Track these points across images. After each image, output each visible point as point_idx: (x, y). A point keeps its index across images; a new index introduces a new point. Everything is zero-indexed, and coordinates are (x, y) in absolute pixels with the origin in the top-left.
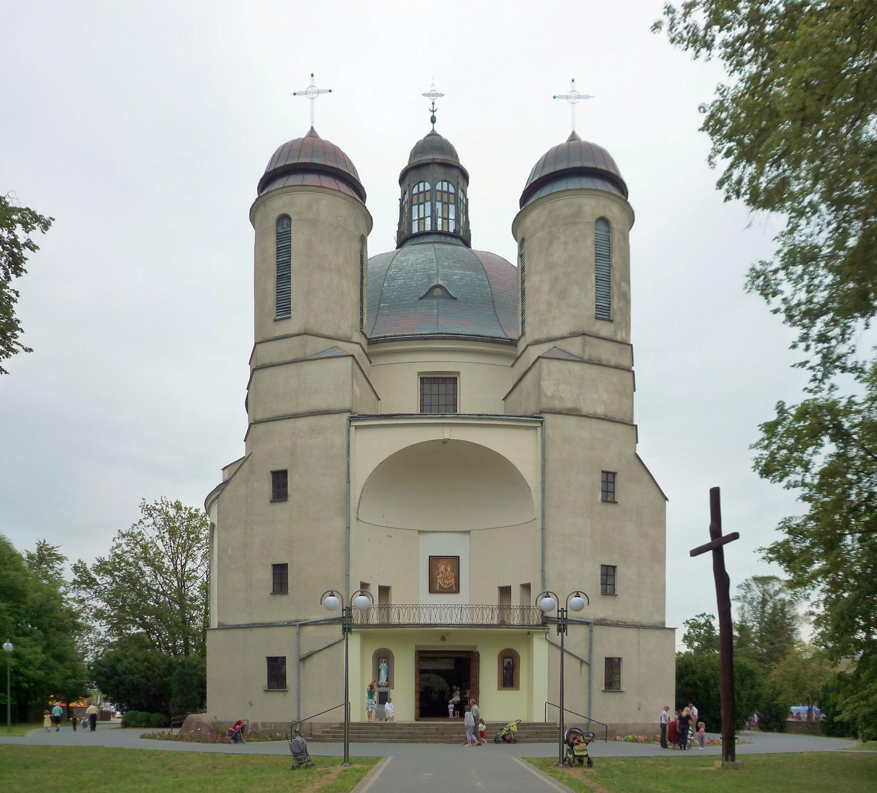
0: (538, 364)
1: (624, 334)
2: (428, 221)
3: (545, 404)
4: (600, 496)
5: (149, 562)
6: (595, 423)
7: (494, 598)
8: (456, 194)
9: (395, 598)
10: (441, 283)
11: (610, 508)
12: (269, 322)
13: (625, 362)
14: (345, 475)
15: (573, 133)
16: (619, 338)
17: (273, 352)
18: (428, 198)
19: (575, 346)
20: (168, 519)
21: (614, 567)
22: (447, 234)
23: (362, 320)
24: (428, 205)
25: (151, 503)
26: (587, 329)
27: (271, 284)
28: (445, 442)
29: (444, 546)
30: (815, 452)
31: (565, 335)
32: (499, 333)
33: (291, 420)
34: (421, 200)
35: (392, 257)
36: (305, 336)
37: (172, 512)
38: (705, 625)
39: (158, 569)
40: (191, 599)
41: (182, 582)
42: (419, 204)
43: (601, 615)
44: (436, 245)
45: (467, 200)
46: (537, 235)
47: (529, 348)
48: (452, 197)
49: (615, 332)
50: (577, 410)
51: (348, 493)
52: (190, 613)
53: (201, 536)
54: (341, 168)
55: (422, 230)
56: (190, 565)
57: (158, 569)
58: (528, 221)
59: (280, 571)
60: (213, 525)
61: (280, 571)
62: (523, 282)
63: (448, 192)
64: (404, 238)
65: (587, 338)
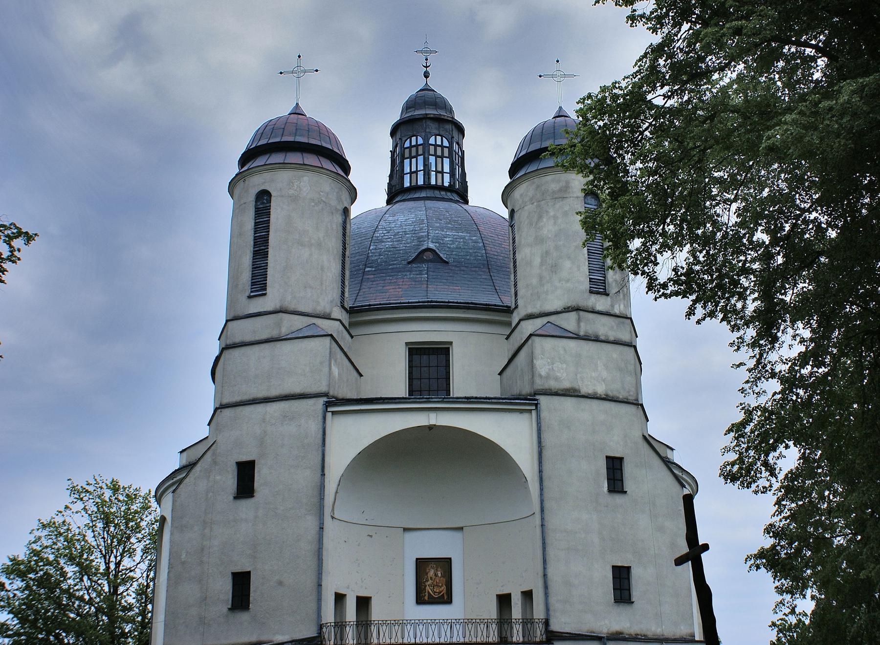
0: (530, 341)
1: (622, 306)
2: (421, 175)
3: (539, 384)
4: (606, 485)
5: (71, 559)
6: (595, 403)
7: (491, 611)
8: (450, 148)
9: (377, 613)
10: (431, 246)
11: (618, 499)
12: (243, 298)
13: (625, 337)
14: (320, 467)
15: (560, 108)
16: (616, 311)
17: (244, 330)
18: (420, 152)
19: (569, 322)
20: (102, 504)
21: (629, 568)
22: (441, 188)
23: (343, 293)
24: (421, 159)
25: (81, 483)
26: (582, 304)
27: (247, 260)
28: (431, 428)
29: (433, 546)
30: (781, 456)
31: (559, 310)
32: (494, 300)
33: (262, 405)
34: (414, 153)
35: (381, 216)
36: (281, 314)
37: (108, 494)
38: (797, 626)
39: (85, 570)
40: (125, 609)
41: (114, 587)
42: (411, 158)
43: (615, 627)
44: (429, 203)
45: (463, 152)
46: (526, 208)
47: (522, 323)
48: (446, 151)
49: (612, 306)
50: (575, 390)
51: (322, 487)
52: (120, 628)
53: (143, 524)
54: (324, 145)
55: (414, 184)
56: (127, 563)
57: (85, 570)
58: (518, 193)
59: (241, 583)
60: (163, 520)
61: (241, 583)
62: (514, 254)
63: (442, 146)
64: (396, 192)
65: (582, 313)
